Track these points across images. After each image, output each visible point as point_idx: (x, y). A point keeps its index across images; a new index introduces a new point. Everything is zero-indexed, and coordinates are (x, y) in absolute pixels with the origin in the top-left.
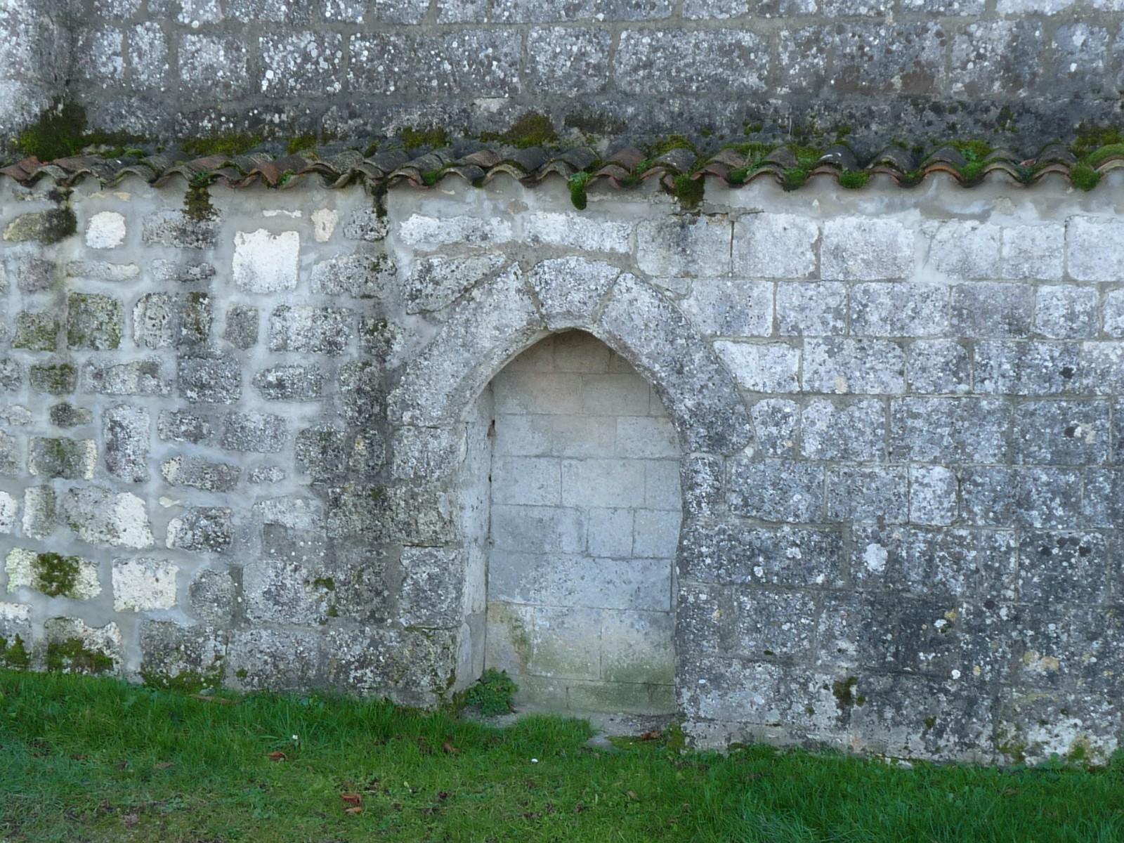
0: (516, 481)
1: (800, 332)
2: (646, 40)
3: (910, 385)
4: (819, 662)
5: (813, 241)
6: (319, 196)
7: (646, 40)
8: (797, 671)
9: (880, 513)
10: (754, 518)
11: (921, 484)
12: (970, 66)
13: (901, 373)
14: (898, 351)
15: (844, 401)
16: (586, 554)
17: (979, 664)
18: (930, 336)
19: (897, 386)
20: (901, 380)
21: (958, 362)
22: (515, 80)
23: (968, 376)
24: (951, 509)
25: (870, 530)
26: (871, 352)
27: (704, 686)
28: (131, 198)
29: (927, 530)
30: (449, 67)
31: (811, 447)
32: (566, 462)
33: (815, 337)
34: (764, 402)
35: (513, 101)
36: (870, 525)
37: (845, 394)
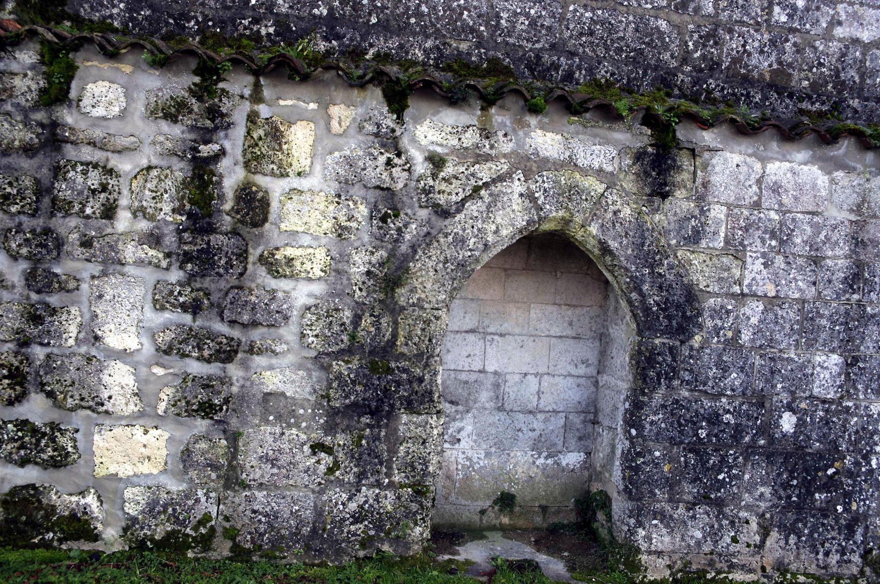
0: (449, 351)
1: (744, 246)
2: (588, 14)
3: (820, 293)
4: (743, 503)
5: (757, 177)
6: (339, 94)
7: (588, 14)
8: (727, 510)
9: (793, 389)
10: (700, 391)
11: (822, 367)
12: (815, 70)
13: (814, 284)
14: (813, 267)
15: (773, 302)
16: (501, 409)
17: (856, 501)
18: (835, 257)
19: (811, 292)
20: (813, 289)
21: (853, 278)
22: (482, 28)
23: (859, 288)
24: (840, 387)
25: (785, 402)
26: (794, 266)
27: (656, 525)
28: (133, 72)
29: (824, 402)
30: (426, 10)
31: (746, 337)
32: (489, 337)
33: (755, 252)
34: (712, 300)
35: (479, 45)
36: (785, 398)
37: (773, 297)
